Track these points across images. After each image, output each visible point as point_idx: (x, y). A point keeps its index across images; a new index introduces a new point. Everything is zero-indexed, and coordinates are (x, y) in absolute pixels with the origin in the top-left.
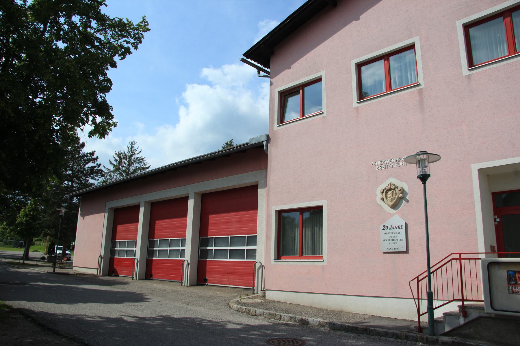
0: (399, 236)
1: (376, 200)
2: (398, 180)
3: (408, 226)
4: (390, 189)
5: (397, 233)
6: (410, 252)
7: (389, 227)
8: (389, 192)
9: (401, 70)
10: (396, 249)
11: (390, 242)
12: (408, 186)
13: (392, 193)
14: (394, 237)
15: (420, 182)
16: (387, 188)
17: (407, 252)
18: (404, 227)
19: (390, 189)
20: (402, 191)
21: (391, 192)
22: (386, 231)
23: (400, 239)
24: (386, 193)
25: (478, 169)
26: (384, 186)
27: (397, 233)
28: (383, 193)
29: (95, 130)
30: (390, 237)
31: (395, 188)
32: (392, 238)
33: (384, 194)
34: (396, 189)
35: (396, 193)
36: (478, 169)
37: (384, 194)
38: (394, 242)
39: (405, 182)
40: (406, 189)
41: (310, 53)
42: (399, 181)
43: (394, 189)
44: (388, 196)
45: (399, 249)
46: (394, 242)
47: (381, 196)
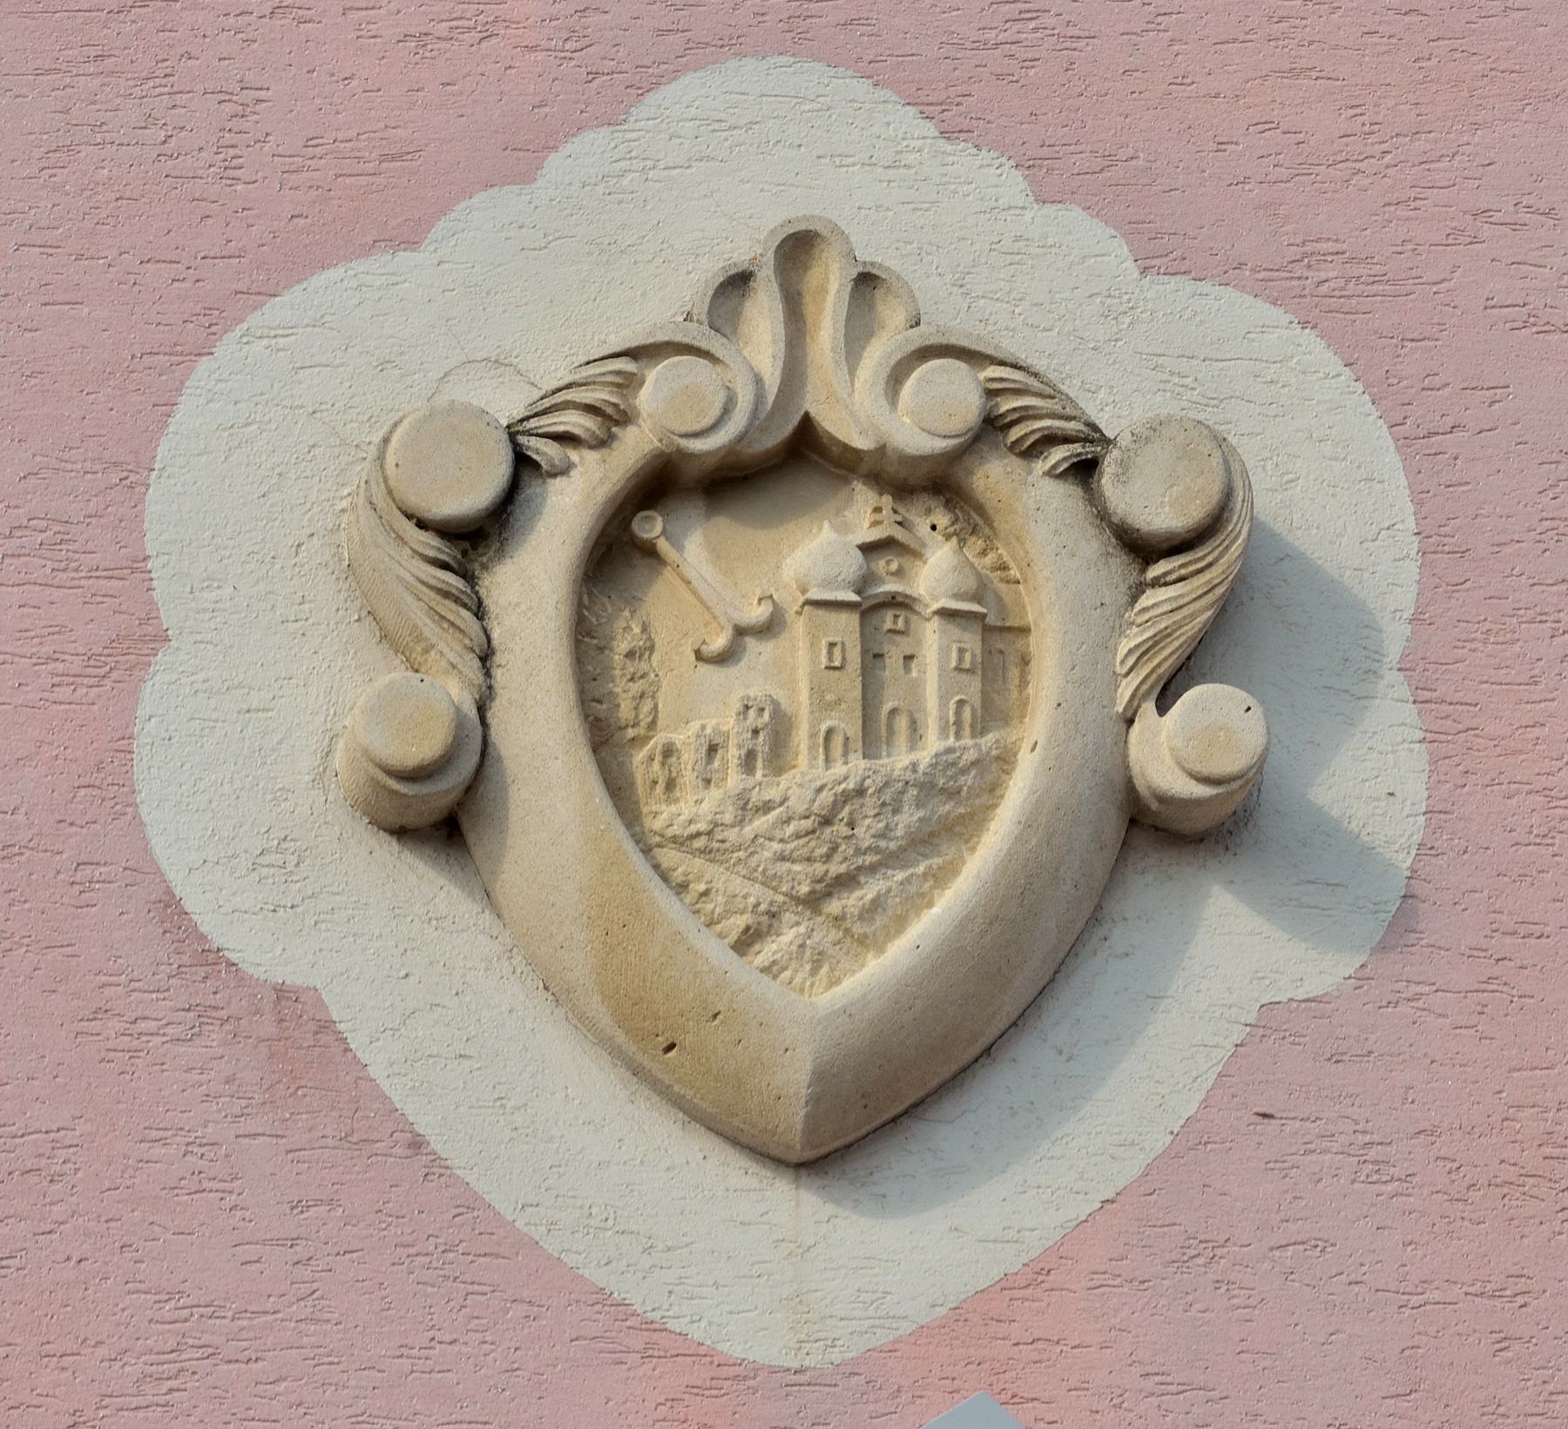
2: (1048, 176)
4: (787, 462)
8: (702, 559)
12: (1417, 443)
13: (877, 609)
15: (419, 879)
19: (787, 462)
20: (1210, 584)
26: (554, 284)
28: (474, 540)
29: (959, 542)
33: (533, 581)
34: (1027, 495)
35: (993, 633)
37: (533, 581)
39: (1306, 283)
40: (1336, 491)
42: (1087, 242)
44: (693, 708)
47: (371, 704)
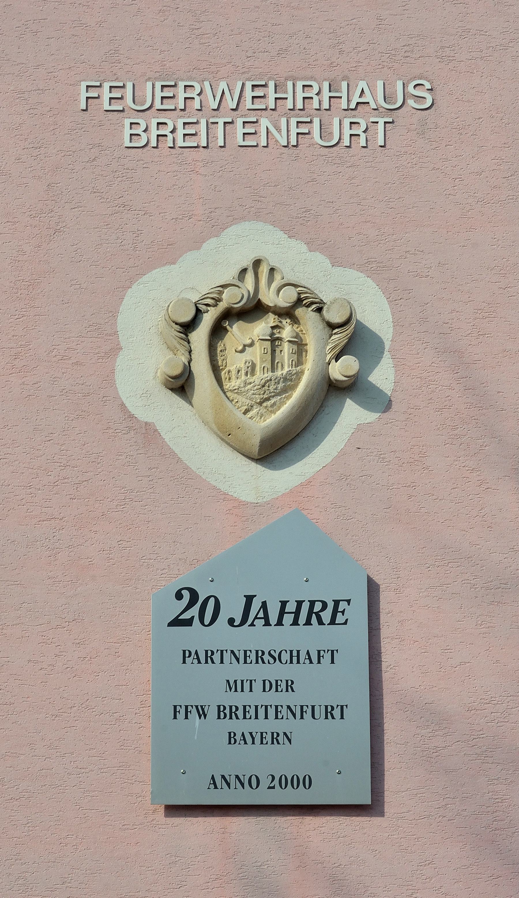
0: (313, 685)
1: (109, 379)
3: (385, 599)
5: (295, 657)
6: (388, 809)
7: (232, 608)
8: (238, 333)
9: (320, 303)
10: (285, 782)
11: (240, 726)
13: (274, 341)
14: (273, 686)
16: (231, 298)
17: (372, 807)
18: (357, 613)
19: (254, 310)
20: (355, 339)
21: (261, 328)
22: (197, 637)
23: (321, 700)
24: (218, 331)
25: (383, 816)
26: (207, 271)
27: (295, 657)
28: (188, 327)
30: (232, 686)
31: (299, 302)
32: (258, 697)
33: (200, 336)
35: (299, 346)
36: (383, 816)
37: (200, 336)
38: (271, 725)
40: (376, 314)
41: (213, 818)
43: (288, 313)
44: (234, 361)
45: (307, 782)
46: (271, 725)
